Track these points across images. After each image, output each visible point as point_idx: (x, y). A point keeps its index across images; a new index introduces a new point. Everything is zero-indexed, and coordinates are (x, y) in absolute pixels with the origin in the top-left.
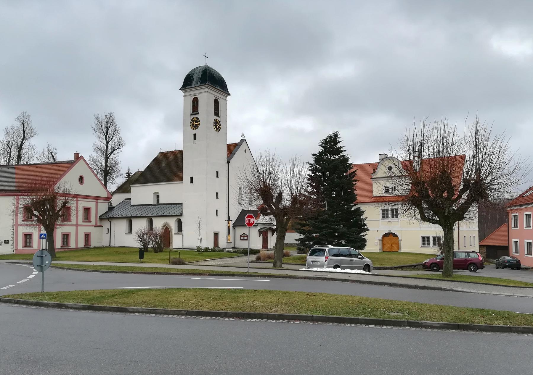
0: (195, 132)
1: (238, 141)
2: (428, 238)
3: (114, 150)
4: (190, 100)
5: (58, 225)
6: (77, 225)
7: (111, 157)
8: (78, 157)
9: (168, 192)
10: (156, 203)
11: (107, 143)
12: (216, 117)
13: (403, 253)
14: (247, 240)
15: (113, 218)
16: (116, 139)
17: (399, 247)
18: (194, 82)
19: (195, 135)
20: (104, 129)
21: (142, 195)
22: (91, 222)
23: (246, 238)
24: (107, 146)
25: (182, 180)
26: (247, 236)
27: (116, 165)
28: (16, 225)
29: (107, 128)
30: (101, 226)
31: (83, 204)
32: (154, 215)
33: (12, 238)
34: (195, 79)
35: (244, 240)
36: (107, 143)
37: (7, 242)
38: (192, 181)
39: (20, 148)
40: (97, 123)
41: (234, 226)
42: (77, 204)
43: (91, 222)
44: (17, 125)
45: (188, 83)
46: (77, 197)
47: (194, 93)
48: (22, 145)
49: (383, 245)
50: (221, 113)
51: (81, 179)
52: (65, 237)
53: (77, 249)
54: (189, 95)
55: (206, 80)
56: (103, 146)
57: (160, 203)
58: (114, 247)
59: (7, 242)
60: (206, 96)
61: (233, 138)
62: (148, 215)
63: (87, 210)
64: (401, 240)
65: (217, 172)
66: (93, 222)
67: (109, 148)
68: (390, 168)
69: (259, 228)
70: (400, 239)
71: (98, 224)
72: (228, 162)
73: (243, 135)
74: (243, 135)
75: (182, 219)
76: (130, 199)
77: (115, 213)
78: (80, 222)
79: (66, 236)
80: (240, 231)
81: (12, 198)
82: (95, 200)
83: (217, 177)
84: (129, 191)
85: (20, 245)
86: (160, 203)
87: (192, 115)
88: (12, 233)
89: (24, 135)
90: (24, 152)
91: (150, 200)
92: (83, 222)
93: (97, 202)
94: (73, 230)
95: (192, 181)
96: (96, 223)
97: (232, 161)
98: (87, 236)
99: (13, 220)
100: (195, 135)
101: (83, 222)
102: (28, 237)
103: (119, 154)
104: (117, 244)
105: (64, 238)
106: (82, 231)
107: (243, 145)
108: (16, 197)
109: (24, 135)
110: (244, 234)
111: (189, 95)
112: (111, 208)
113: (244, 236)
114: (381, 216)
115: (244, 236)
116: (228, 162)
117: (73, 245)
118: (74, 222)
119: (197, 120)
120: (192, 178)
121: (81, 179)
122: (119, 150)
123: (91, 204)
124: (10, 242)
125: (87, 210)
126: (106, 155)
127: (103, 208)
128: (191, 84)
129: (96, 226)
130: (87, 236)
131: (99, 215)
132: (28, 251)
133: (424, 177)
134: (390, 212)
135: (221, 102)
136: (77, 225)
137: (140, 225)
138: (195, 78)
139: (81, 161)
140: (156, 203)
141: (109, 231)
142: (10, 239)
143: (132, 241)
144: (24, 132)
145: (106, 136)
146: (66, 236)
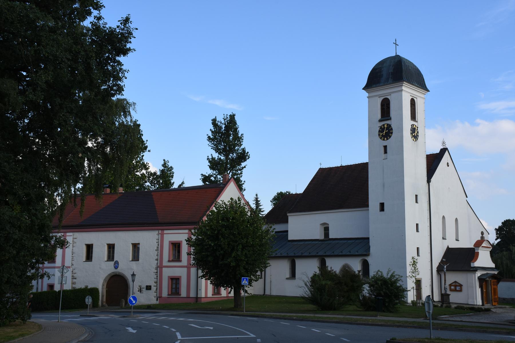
0: (385, 143)
1: (437, 151)
4: (379, 101)
9: (341, 223)
10: (322, 237)
12: (413, 123)
14: (461, 291)
19: (385, 147)
21: (302, 227)
22: (180, 261)
25: (367, 206)
26: (461, 286)
28: (160, 267)
32: (327, 254)
33: (156, 282)
35: (455, 290)
37: (149, 288)
41: (440, 269)
43: (180, 261)
52: (174, 282)
54: (376, 96)
55: (391, 74)
57: (330, 237)
58: (271, 297)
62: (319, 254)
65: (416, 196)
69: (479, 274)
72: (429, 181)
73: (444, 143)
74: (444, 143)
75: (369, 259)
80: (451, 278)
81: (157, 232)
82: (187, 231)
83: (417, 202)
84: (286, 221)
85: (165, 293)
86: (330, 237)
87: (380, 121)
88: (155, 276)
91: (318, 235)
92: (169, 261)
99: (157, 260)
100: (385, 147)
104: (274, 293)
107: (446, 158)
108: (160, 231)
110: (455, 282)
111: (376, 96)
115: (455, 286)
116: (429, 181)
119: (389, 127)
124: (152, 287)
132: (174, 300)
133: (36, 80)
137: (308, 268)
138: (384, 73)
142: (153, 284)
143: (298, 288)
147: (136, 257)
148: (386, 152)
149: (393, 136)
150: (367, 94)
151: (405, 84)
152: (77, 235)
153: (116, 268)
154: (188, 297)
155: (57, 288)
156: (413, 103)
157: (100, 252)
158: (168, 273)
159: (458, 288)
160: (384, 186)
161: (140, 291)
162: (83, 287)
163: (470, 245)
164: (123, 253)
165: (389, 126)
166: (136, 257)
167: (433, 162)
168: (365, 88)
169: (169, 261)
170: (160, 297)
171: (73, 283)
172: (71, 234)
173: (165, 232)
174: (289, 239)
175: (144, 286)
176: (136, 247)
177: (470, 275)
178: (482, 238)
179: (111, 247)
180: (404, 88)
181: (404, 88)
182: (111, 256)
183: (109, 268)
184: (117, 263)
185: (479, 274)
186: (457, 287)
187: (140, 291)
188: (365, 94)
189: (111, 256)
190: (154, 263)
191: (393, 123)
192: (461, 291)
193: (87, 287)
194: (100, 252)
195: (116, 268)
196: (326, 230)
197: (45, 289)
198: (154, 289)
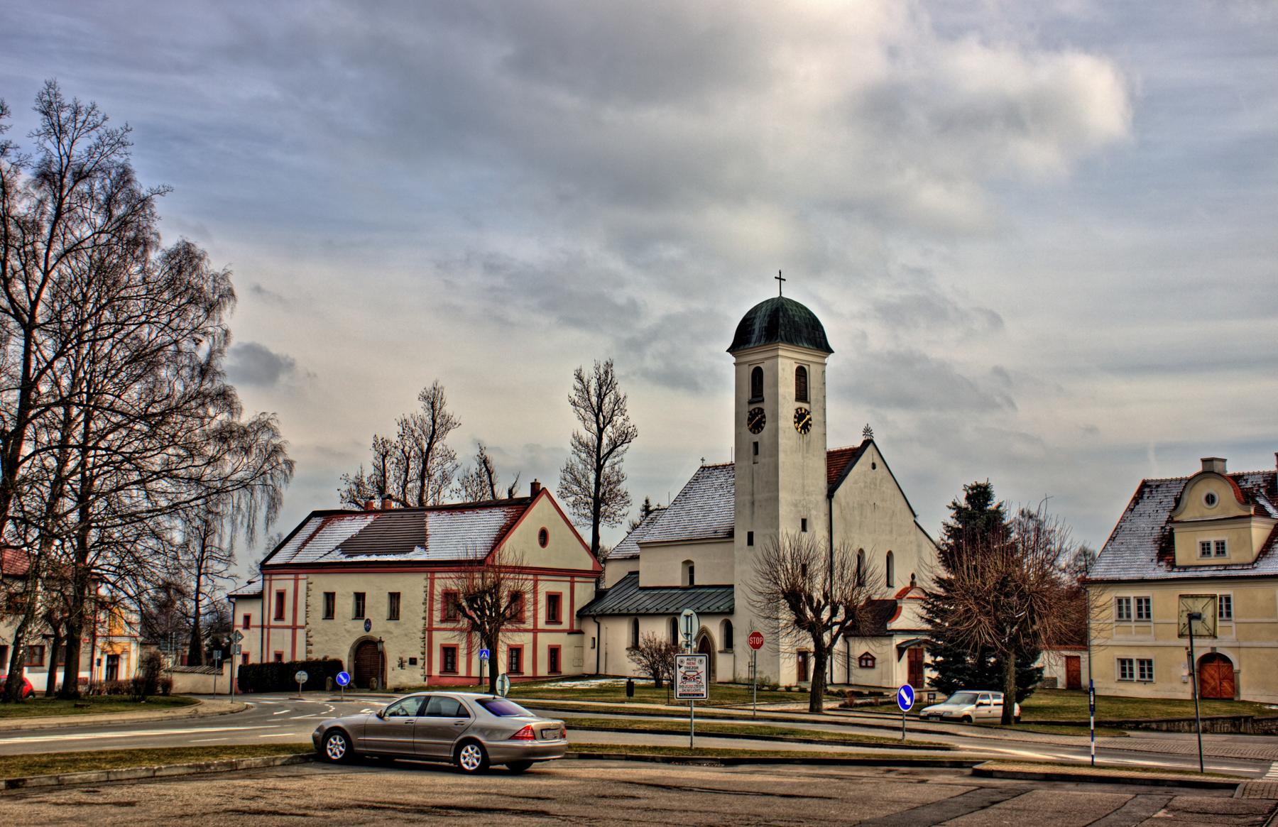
0: (756, 438)
2: (1131, 661)
3: (615, 447)
4: (748, 372)
5: (296, 580)
6: (535, 631)
7: (607, 463)
8: (537, 491)
10: (687, 584)
11: (601, 431)
13: (1244, 702)
14: (873, 667)
15: (604, 615)
16: (618, 420)
17: (1235, 690)
18: (754, 337)
19: (756, 444)
20: (594, 399)
22: (561, 623)
23: (870, 663)
24: (600, 439)
26: (873, 659)
27: (619, 481)
28: (429, 630)
29: (601, 398)
30: (580, 632)
31: (546, 586)
34: (757, 332)
35: (867, 667)
36: (601, 431)
37: (413, 661)
38: (750, 542)
39: (425, 456)
40: (579, 386)
42: (535, 586)
43: (561, 623)
44: (420, 410)
45: (743, 339)
46: (538, 572)
47: (755, 357)
48: (429, 449)
49: (1203, 682)
50: (813, 394)
51: (543, 536)
53: (536, 679)
56: (589, 436)
59: (413, 661)
60: (785, 363)
61: (842, 437)
63: (554, 600)
64: (1239, 672)
66: (566, 624)
67: (605, 441)
68: (1210, 499)
69: (898, 640)
70: (1236, 667)
71: (575, 628)
72: (830, 495)
76: (637, 573)
77: (608, 604)
78: (541, 623)
79: (516, 652)
81: (424, 576)
87: (750, 403)
89: (434, 430)
90: (433, 464)
91: (676, 578)
92: (442, 621)
93: (572, 583)
94: (531, 640)
95: (750, 542)
96: (572, 625)
97: (840, 492)
98: (554, 652)
100: (756, 444)
101: (547, 623)
102: (449, 653)
103: (625, 456)
105: (512, 657)
106: (545, 641)
107: (868, 456)
109: (434, 430)
110: (867, 653)
112: (600, 595)
113: (867, 660)
114: (1118, 675)
116: (830, 495)
117: (527, 670)
118: (529, 625)
120: (750, 535)
121: (543, 536)
122: (625, 446)
123: (562, 587)
125: (554, 600)
126: (598, 460)
127: (584, 593)
128: (748, 342)
129: (571, 632)
130: (554, 652)
131: (577, 608)
134: (1136, 667)
135: (813, 372)
136: (535, 631)
139: (544, 498)
140: (687, 584)
141: (596, 643)
142: (418, 656)
144: (434, 422)
145: (597, 416)
146: (516, 652)
147: (394, 614)
148: (756, 453)
149: (767, 427)
150: (734, 360)
151: (781, 346)
152: (312, 578)
153: (368, 629)
154: (468, 677)
155: (287, 659)
156: (801, 373)
157: (345, 606)
158: (440, 638)
159: (870, 663)
160: (753, 503)
161: (401, 665)
162: (321, 657)
163: (891, 595)
164: (377, 608)
165: (761, 410)
166: (394, 614)
167: (840, 464)
168: (731, 350)
169: (442, 621)
170: (430, 676)
171: (309, 652)
172: (304, 576)
173: (437, 575)
174: (641, 584)
175: (406, 658)
176: (395, 597)
177: (885, 641)
178: (913, 584)
179: (360, 597)
180: (780, 352)
181: (780, 352)
182: (359, 613)
183: (358, 629)
184: (368, 622)
185: (898, 640)
186: (867, 661)
187: (401, 665)
188: (732, 359)
189: (359, 613)
190: (421, 624)
191: (767, 406)
192: (873, 667)
193: (325, 658)
194: (345, 606)
195: (368, 629)
196: (690, 567)
197: (272, 659)
198: (420, 663)
